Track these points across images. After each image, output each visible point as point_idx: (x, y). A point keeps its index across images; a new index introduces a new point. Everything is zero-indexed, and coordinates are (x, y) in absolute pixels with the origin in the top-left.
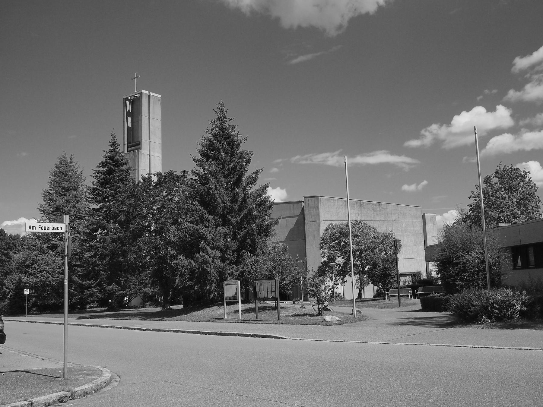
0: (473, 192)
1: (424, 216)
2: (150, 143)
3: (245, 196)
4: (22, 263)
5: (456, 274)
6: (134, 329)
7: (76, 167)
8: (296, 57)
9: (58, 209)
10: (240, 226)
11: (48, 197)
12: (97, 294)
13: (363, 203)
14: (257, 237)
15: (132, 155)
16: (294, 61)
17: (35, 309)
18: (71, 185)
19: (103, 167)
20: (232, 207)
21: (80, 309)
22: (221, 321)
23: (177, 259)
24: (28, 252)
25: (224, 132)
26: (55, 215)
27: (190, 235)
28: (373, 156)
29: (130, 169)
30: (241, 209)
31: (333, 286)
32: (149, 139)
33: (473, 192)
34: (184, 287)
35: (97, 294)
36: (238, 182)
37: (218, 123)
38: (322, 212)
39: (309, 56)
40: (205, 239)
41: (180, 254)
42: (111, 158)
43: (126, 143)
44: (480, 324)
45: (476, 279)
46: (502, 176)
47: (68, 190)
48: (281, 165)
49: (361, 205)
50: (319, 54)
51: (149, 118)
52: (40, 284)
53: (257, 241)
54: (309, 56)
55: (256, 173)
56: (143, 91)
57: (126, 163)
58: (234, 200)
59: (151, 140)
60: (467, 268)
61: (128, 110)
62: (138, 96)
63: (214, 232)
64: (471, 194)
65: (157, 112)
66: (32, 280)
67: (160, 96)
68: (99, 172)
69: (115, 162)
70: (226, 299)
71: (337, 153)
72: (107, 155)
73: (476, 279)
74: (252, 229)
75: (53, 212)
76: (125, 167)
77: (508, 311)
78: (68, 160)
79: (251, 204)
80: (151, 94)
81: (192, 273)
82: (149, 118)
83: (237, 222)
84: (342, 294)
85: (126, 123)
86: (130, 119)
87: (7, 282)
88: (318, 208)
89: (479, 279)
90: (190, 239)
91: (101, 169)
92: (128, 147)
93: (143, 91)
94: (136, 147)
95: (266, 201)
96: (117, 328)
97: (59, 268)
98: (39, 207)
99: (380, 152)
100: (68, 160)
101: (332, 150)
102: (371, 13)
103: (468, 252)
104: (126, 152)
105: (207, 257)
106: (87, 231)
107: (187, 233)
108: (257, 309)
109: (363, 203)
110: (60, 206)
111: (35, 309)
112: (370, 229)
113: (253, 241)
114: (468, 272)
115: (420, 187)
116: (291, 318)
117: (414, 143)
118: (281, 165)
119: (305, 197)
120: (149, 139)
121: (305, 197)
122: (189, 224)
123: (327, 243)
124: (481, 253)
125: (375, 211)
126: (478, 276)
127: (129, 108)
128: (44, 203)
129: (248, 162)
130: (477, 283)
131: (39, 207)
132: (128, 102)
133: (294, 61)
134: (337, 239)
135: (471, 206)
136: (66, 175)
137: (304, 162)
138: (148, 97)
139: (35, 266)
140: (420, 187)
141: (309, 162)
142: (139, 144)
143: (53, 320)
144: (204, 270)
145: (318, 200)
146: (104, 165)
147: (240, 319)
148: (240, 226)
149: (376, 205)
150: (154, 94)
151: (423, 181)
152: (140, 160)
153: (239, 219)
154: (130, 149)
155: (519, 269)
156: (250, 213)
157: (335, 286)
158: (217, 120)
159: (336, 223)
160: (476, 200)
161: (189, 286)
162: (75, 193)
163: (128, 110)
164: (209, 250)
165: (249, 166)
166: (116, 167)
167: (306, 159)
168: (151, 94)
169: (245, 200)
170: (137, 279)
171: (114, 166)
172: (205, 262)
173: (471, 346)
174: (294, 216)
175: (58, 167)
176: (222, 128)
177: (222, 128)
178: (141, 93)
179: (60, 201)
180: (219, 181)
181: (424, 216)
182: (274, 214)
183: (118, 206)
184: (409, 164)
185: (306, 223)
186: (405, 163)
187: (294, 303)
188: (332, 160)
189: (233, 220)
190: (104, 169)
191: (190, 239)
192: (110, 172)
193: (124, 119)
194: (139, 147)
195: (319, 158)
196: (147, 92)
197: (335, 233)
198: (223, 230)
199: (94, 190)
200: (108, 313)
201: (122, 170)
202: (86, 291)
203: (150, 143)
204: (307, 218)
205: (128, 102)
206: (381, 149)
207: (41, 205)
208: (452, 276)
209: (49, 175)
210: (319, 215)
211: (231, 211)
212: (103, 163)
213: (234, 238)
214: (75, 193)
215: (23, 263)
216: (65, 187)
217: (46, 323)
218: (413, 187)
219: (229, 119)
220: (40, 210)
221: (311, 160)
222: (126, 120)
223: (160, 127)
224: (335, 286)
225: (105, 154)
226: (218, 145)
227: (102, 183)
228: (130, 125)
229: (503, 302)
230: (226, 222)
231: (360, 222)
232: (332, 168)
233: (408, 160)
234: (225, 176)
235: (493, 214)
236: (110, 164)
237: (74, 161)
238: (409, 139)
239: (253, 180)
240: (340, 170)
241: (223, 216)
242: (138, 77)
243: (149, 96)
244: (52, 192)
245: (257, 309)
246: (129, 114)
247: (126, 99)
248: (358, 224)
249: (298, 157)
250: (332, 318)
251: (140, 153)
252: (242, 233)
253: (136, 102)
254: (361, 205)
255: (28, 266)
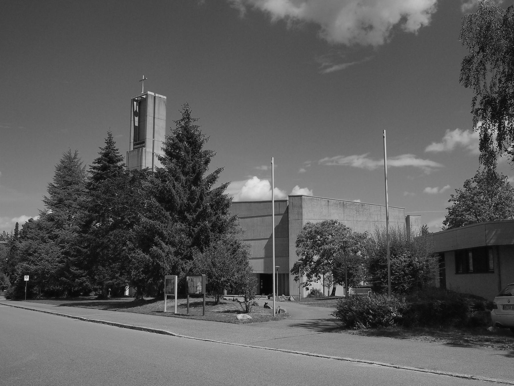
0: (453, 196)
1: (407, 219)
2: (154, 141)
3: (201, 194)
4: (25, 251)
5: (383, 277)
6: (78, 318)
7: (79, 163)
8: (331, 66)
9: (60, 201)
10: (195, 222)
11: (52, 190)
12: (87, 283)
13: (346, 203)
14: (211, 234)
15: (137, 152)
16: (328, 70)
17: (42, 294)
18: (74, 179)
19: (99, 163)
20: (188, 204)
21: (83, 295)
22: (160, 314)
23: (135, 252)
24: (30, 241)
25: (187, 132)
26: (57, 207)
27: (148, 230)
28: (398, 159)
29: (123, 165)
30: (198, 206)
31: (307, 283)
32: (154, 138)
33: (453, 196)
34: (139, 280)
35: (87, 283)
36: (197, 180)
37: (183, 123)
38: (305, 211)
39: (343, 66)
40: (161, 235)
41: (137, 248)
42: (106, 155)
43: (132, 141)
44: (355, 329)
45: (402, 283)
46: (481, 180)
47: (70, 184)
48: (309, 165)
49: (344, 205)
50: (353, 63)
51: (154, 118)
52: (40, 272)
53: (211, 237)
54: (343, 66)
55: (217, 172)
56: (149, 93)
57: (119, 160)
58: (191, 199)
59: (156, 139)
60: (393, 272)
61: (135, 110)
62: (144, 97)
63: (175, 228)
64: (451, 198)
65: (162, 112)
66: (33, 268)
67: (165, 97)
68: (94, 168)
69: (109, 158)
70: (166, 293)
71: (364, 155)
72: (103, 152)
73: (402, 283)
74: (205, 225)
75: (56, 204)
76: (119, 164)
77: (383, 317)
78: (73, 155)
79: (207, 202)
80: (157, 95)
81: (147, 266)
82: (154, 118)
83: (193, 218)
84: (322, 291)
85: (133, 122)
86: (137, 119)
87: (18, 269)
88: (301, 207)
89: (405, 283)
90: (146, 234)
91: (97, 165)
92: (134, 145)
93: (149, 93)
94: (141, 145)
95: (223, 198)
96: (68, 316)
97: (58, 257)
98: (44, 199)
99: (406, 155)
100: (73, 155)
101: (358, 152)
102: (412, 26)
103: (395, 255)
104: (132, 149)
105: (160, 251)
106: (83, 223)
107: (145, 228)
108: (205, 303)
109: (346, 203)
110: (62, 199)
111: (42, 294)
112: (345, 229)
113: (207, 237)
114: (394, 275)
115: (442, 191)
116: (223, 315)
117: (435, 147)
118: (309, 165)
119: (289, 196)
120: (154, 138)
121: (289, 196)
122: (148, 220)
123: (303, 241)
124: (409, 257)
125: (358, 211)
126: (403, 280)
127: (136, 108)
128: (49, 196)
129: (207, 162)
130: (403, 286)
131: (44, 199)
132: (135, 103)
133: (328, 70)
134: (315, 237)
135: (449, 209)
136: (70, 170)
137: (330, 164)
138: (153, 98)
139: (36, 254)
140: (442, 191)
141: (334, 164)
142: (144, 142)
143: (35, 306)
144: (158, 264)
145: (301, 199)
146: (99, 161)
147: (176, 313)
148: (195, 222)
149: (359, 205)
150: (160, 96)
151: (446, 186)
152: (144, 157)
153: (194, 216)
154: (136, 146)
155: (471, 273)
156: (205, 210)
157: (308, 283)
158: (182, 120)
159: (314, 222)
160: (455, 204)
161: (143, 278)
162: (76, 187)
163: (135, 110)
164: (164, 245)
165: (209, 165)
166: (110, 163)
167: (332, 162)
168: (157, 95)
169: (201, 198)
170: (107, 270)
171: (109, 162)
172: (159, 257)
173: (306, 353)
174: (281, 215)
175: (63, 162)
176: (186, 129)
177: (186, 129)
178: (147, 95)
179: (63, 194)
180: (177, 179)
181: (407, 219)
182: (231, 212)
183: (94, 200)
184: (432, 168)
185: (290, 221)
186: (428, 166)
187: (269, 298)
188: (358, 161)
189: (189, 217)
190: (99, 165)
191: (146, 234)
192: (104, 168)
193: (131, 118)
194: (143, 144)
195: (344, 161)
196: (153, 94)
197: (311, 231)
198: (178, 225)
199: (90, 184)
200: (97, 301)
201: (116, 167)
202: (77, 280)
203: (154, 141)
204: (291, 217)
205: (135, 103)
206: (407, 153)
207: (45, 197)
208: (379, 279)
209: (55, 169)
210: (302, 214)
211: (189, 209)
212: (98, 159)
213: (190, 235)
214: (76, 187)
215: (26, 251)
216: (67, 181)
217: (26, 309)
218: (435, 190)
219: (193, 119)
220: (45, 202)
221: (337, 162)
222: (133, 119)
223: (165, 127)
224: (308, 283)
225: (100, 150)
226: (180, 144)
227: (97, 178)
228: (137, 124)
229: (380, 308)
230: (184, 219)
231: (336, 222)
232: (357, 170)
233: (432, 164)
234: (185, 174)
235: (470, 217)
236: (105, 160)
237: (78, 157)
238: (430, 143)
239: (212, 179)
240: (362, 171)
241: (181, 213)
242: (145, 79)
243: (155, 97)
244: (56, 185)
245: (205, 303)
246: (136, 114)
247: (134, 100)
248: (334, 224)
249: (326, 159)
250: (243, 317)
251: (144, 150)
252: (196, 230)
253: (142, 103)
254: (344, 205)
255: (30, 255)
